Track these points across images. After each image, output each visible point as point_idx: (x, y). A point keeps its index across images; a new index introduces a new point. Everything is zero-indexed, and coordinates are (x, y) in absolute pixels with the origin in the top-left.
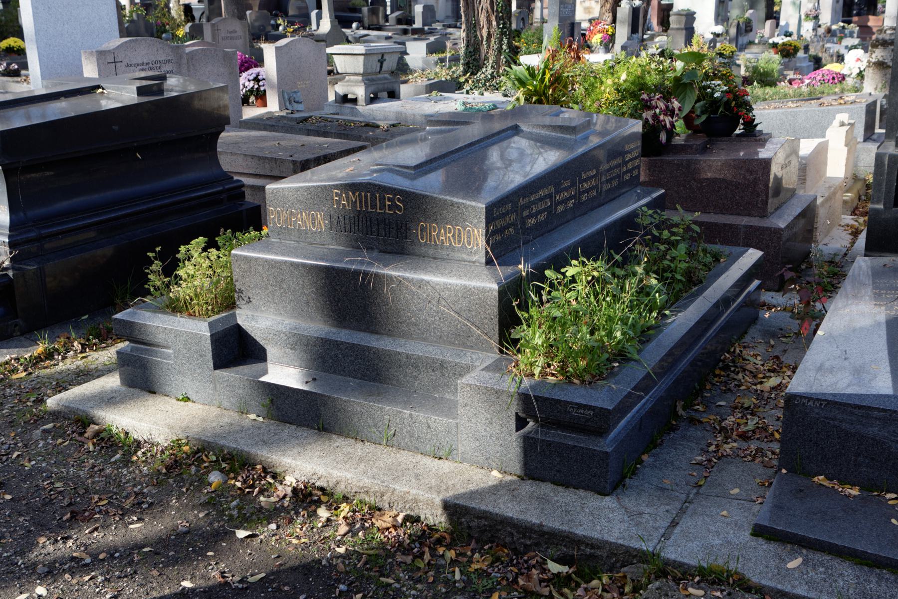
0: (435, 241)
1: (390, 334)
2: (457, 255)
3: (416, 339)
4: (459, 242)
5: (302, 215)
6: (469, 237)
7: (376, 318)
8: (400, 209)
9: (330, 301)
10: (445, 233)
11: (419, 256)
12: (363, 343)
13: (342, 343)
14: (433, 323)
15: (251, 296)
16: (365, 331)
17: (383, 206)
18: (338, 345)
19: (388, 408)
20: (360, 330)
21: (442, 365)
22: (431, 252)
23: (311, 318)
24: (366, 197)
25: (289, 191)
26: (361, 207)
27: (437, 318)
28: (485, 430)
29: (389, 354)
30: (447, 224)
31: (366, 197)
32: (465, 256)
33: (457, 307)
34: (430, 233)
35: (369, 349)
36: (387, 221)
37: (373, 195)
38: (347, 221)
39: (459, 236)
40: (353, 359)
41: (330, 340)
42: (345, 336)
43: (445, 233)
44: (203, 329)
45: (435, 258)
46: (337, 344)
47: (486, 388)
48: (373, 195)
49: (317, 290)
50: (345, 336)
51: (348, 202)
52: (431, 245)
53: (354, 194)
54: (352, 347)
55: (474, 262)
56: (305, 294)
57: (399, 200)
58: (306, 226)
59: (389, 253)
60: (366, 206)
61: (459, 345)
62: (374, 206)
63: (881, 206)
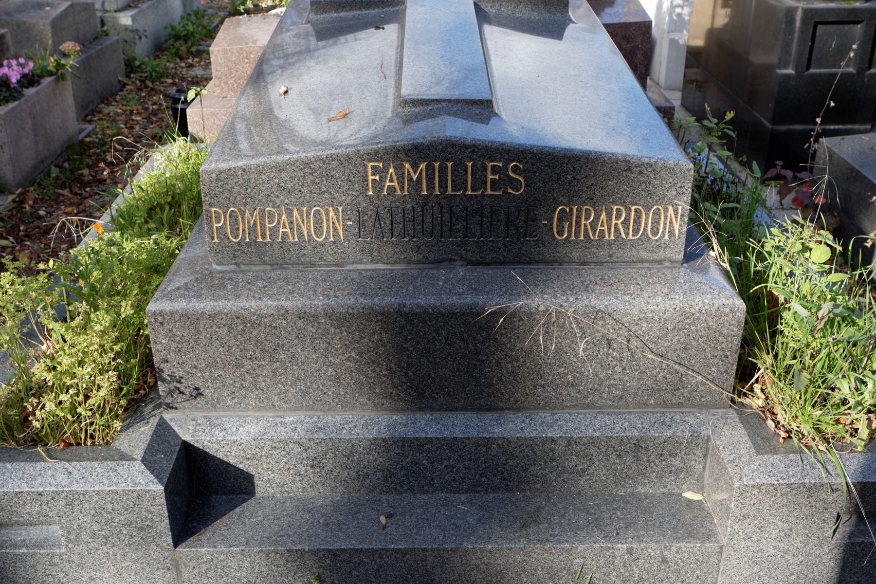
0: (586, 235)
1: (517, 407)
2: (629, 254)
3: (570, 407)
4: (636, 231)
5: (290, 214)
6: (656, 222)
7: (489, 386)
8: (515, 185)
9: (389, 369)
10: (609, 219)
11: (550, 263)
12: (474, 434)
13: (430, 440)
14: (609, 378)
15: (199, 384)
16: (464, 409)
17: (480, 182)
18: (422, 445)
19: (581, 547)
20: (454, 409)
21: (638, 446)
22: (603, 253)
23: (345, 406)
24: (443, 170)
25: (260, 173)
26: (430, 188)
27: (618, 369)
28: (775, 548)
29: (531, 443)
30: (614, 203)
31: (443, 170)
32: (644, 254)
33: (663, 346)
34: (578, 223)
35: (488, 442)
36: (487, 210)
37: (459, 167)
38: (398, 218)
39: (637, 222)
40: (452, 462)
41: (404, 440)
42: (428, 426)
43: (609, 219)
44: (140, 479)
45: (584, 263)
46: (418, 445)
47: (789, 486)
48: (459, 167)
49: (360, 354)
50: (428, 426)
51: (401, 183)
52: (576, 242)
53: (415, 166)
54: (452, 444)
55: (660, 262)
56: (331, 364)
57: (515, 169)
58: (300, 235)
59: (488, 264)
60: (443, 185)
61: (656, 405)
62: (459, 185)
63: (790, 71)
